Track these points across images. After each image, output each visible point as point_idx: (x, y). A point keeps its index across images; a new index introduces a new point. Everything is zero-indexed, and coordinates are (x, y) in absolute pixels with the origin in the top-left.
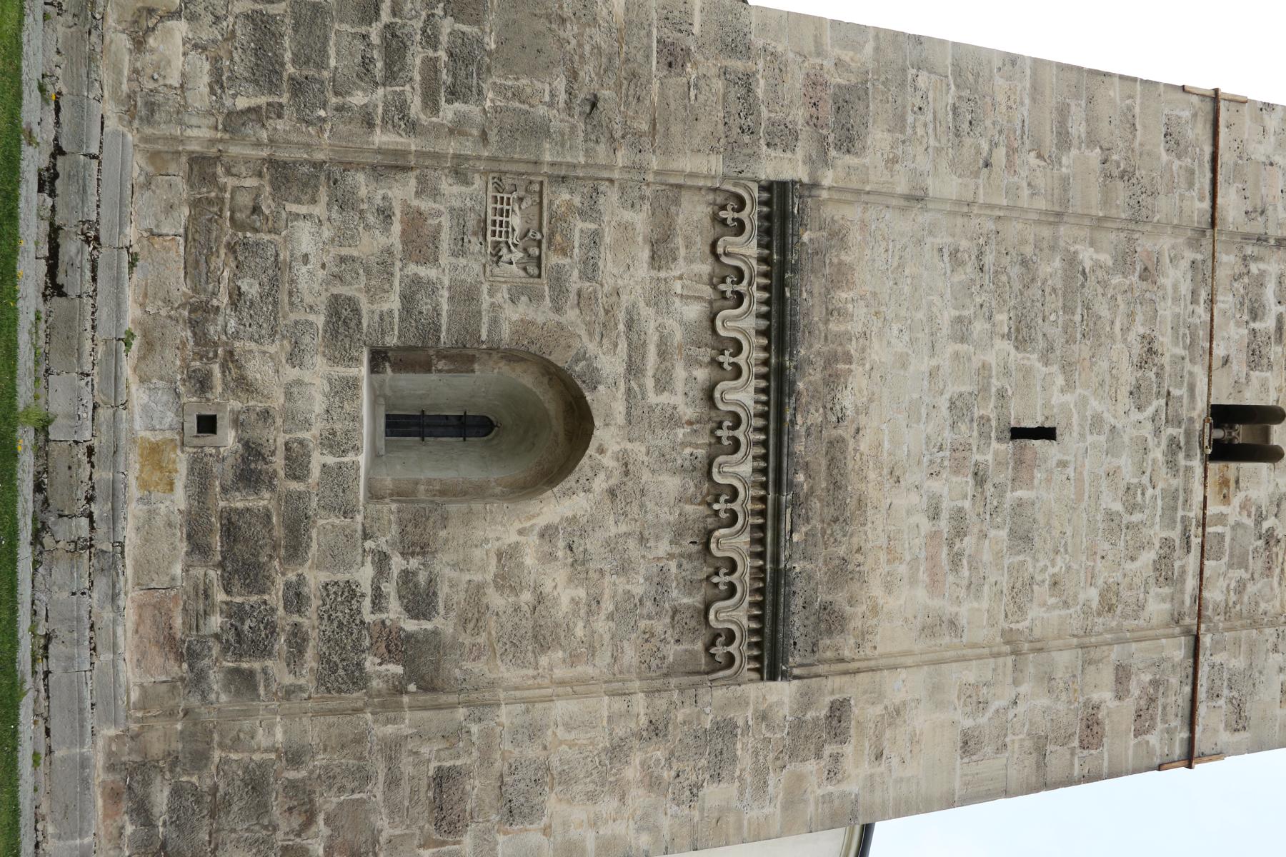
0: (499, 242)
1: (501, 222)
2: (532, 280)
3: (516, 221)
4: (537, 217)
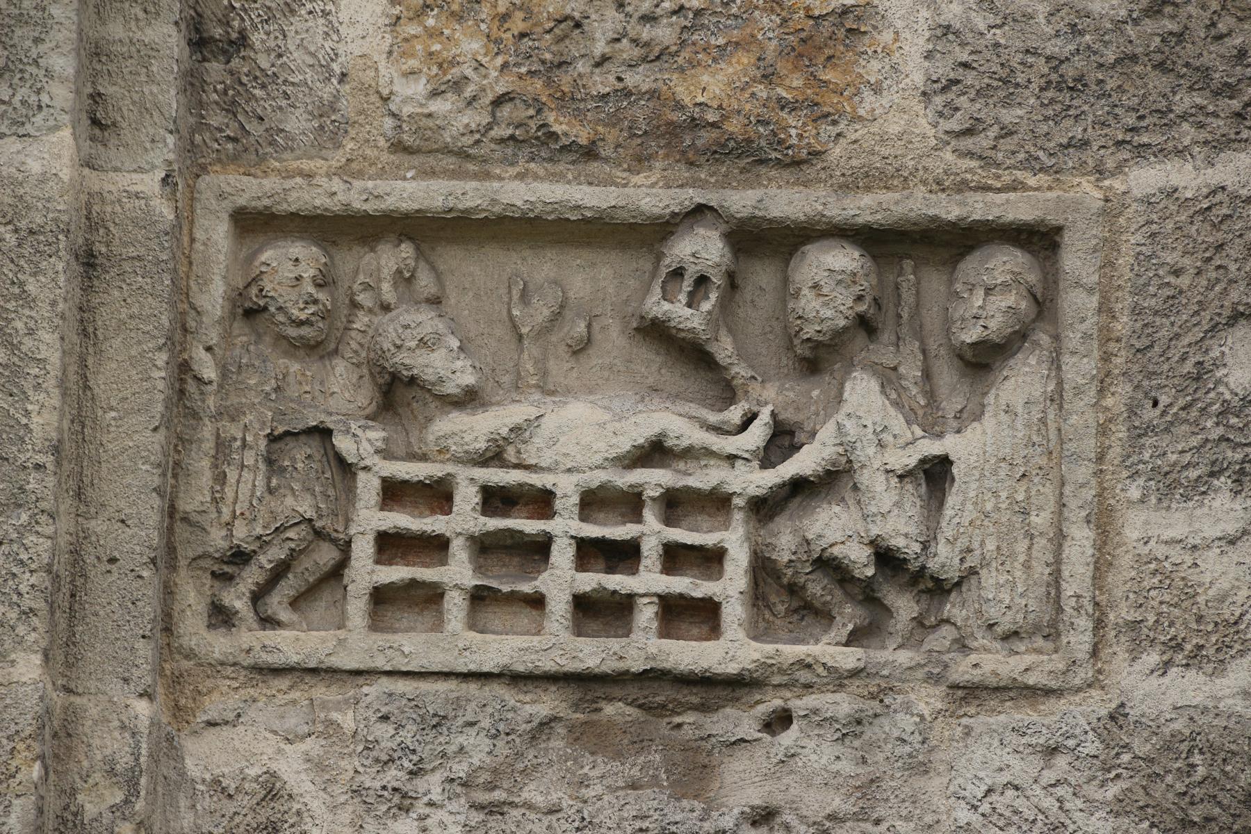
0: (763, 569)
1: (591, 552)
2: (1078, 304)
3: (581, 432)
4: (541, 267)
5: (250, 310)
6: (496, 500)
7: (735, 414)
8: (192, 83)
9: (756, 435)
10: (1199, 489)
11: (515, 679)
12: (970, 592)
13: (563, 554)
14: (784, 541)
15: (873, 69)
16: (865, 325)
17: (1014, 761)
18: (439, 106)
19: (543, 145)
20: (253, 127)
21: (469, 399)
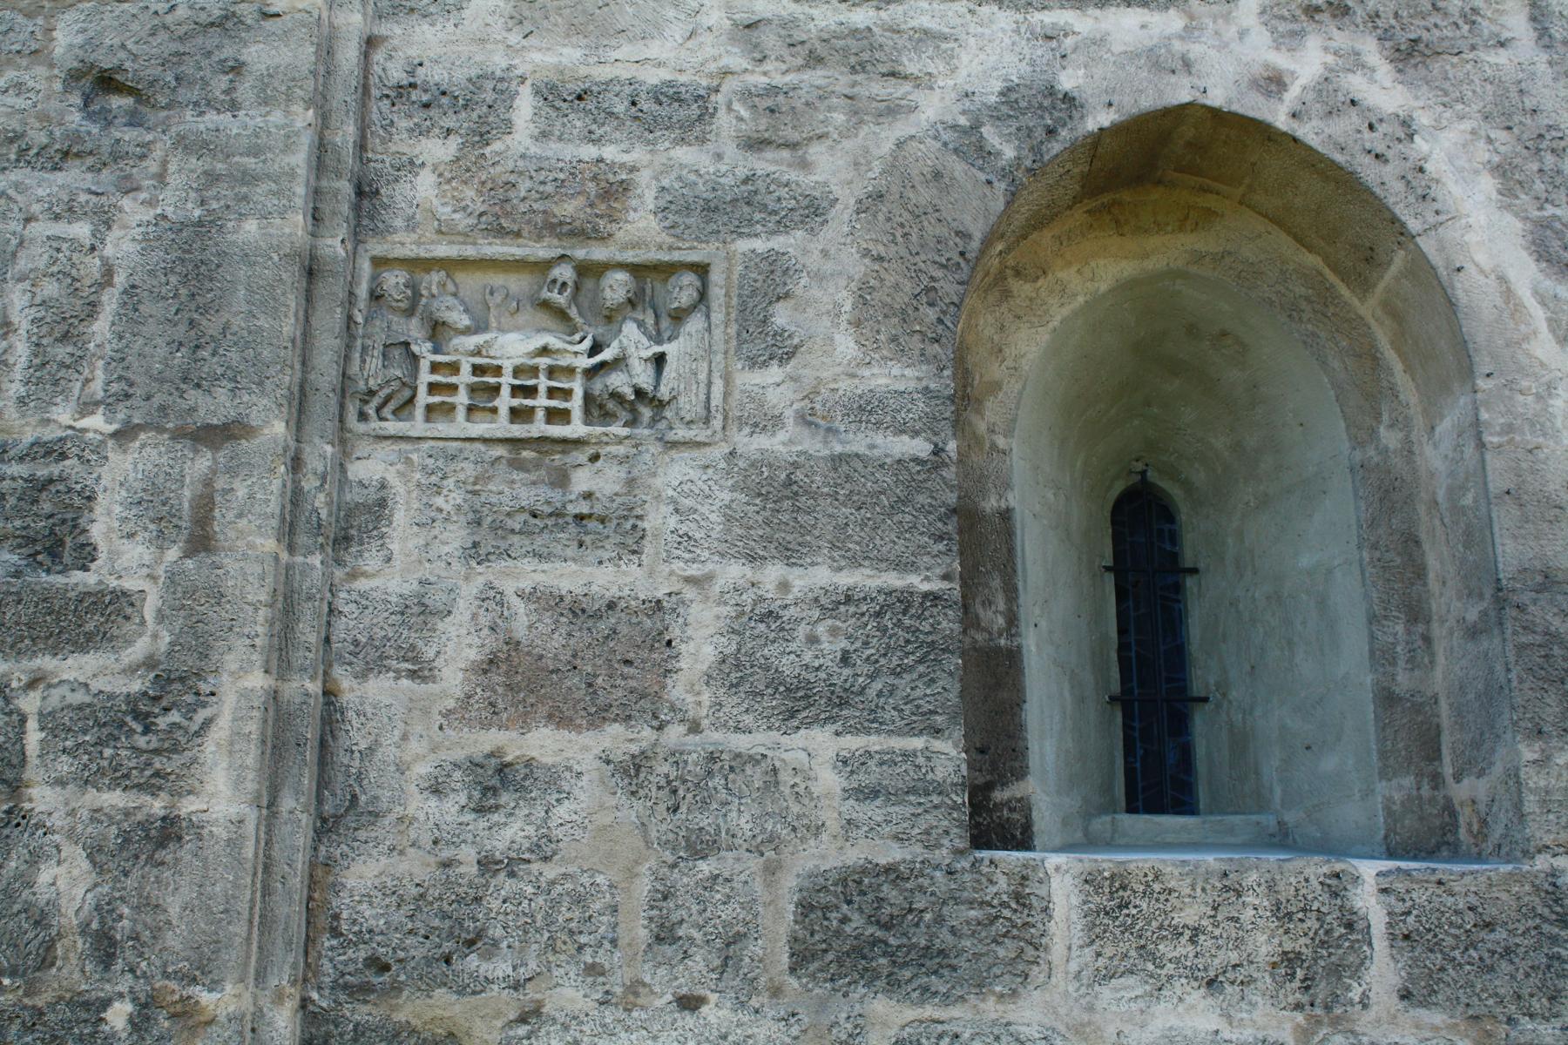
0: (588, 398)
2: (717, 293)
3: (513, 346)
5: (376, 296)
6: (478, 370)
7: (577, 337)
8: (357, 208)
9: (587, 343)
10: (765, 364)
11: (485, 441)
12: (673, 406)
13: (505, 391)
14: (597, 386)
15: (634, 203)
16: (631, 303)
17: (688, 470)
18: (457, 216)
19: (500, 232)
20: (380, 225)
21: (467, 331)
